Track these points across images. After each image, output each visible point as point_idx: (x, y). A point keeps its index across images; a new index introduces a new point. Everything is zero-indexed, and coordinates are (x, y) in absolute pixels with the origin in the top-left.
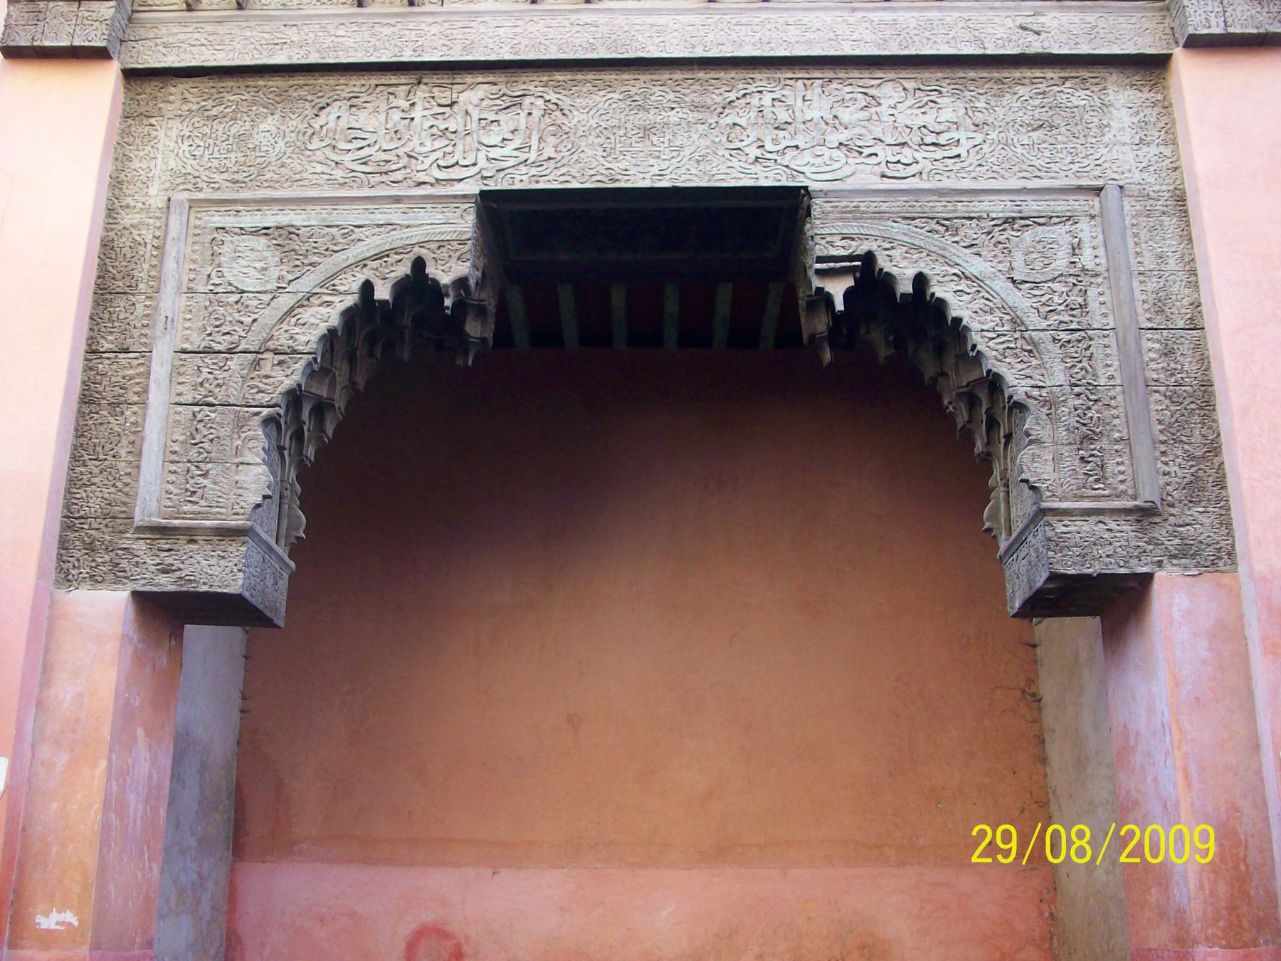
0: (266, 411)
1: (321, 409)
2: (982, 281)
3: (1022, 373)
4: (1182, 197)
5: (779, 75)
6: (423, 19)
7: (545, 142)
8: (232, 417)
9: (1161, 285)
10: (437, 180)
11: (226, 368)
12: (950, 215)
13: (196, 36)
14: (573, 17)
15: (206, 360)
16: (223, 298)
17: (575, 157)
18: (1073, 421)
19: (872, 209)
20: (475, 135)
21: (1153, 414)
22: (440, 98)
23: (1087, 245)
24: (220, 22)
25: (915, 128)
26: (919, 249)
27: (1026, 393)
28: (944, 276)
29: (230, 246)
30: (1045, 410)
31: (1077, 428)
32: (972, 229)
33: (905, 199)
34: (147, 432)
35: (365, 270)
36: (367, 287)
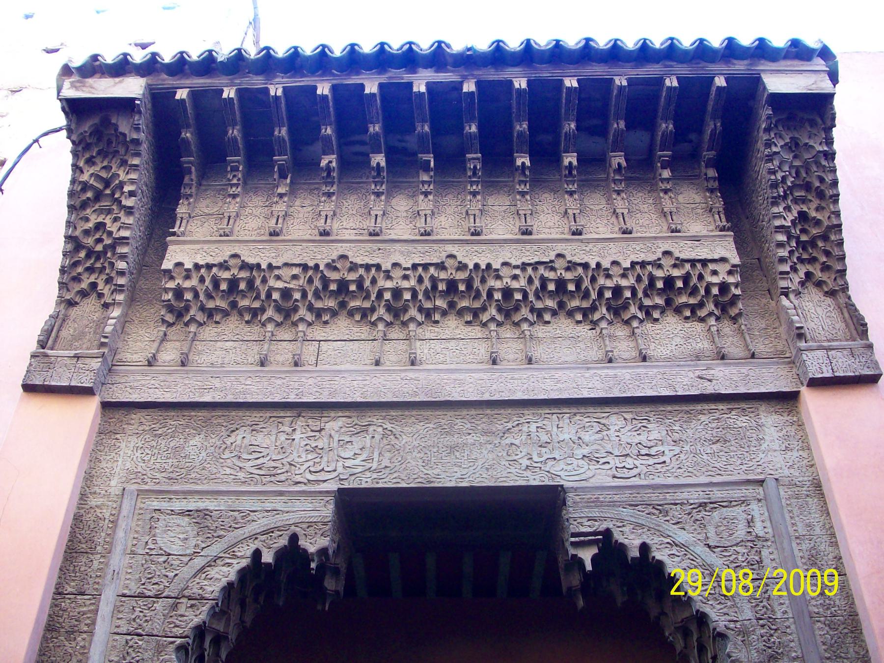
0: (179, 641)
1: (218, 639)
2: (688, 547)
3: (721, 611)
4: (818, 484)
5: (540, 411)
6: (303, 375)
7: (383, 456)
8: (154, 644)
9: (812, 545)
10: (308, 480)
11: (153, 608)
12: (661, 503)
13: (153, 382)
14: (403, 375)
15: (139, 602)
16: (155, 558)
17: (404, 466)
18: (761, 645)
19: (607, 500)
20: (335, 451)
21: (818, 637)
22: (313, 426)
23: (758, 520)
24: (170, 373)
25: (634, 444)
26: (642, 526)
27: (725, 626)
28: (661, 545)
29: (164, 522)
30: (740, 638)
31: (765, 650)
32: (677, 511)
33: (630, 492)
34: (91, 653)
35: (256, 542)
36: (257, 554)
